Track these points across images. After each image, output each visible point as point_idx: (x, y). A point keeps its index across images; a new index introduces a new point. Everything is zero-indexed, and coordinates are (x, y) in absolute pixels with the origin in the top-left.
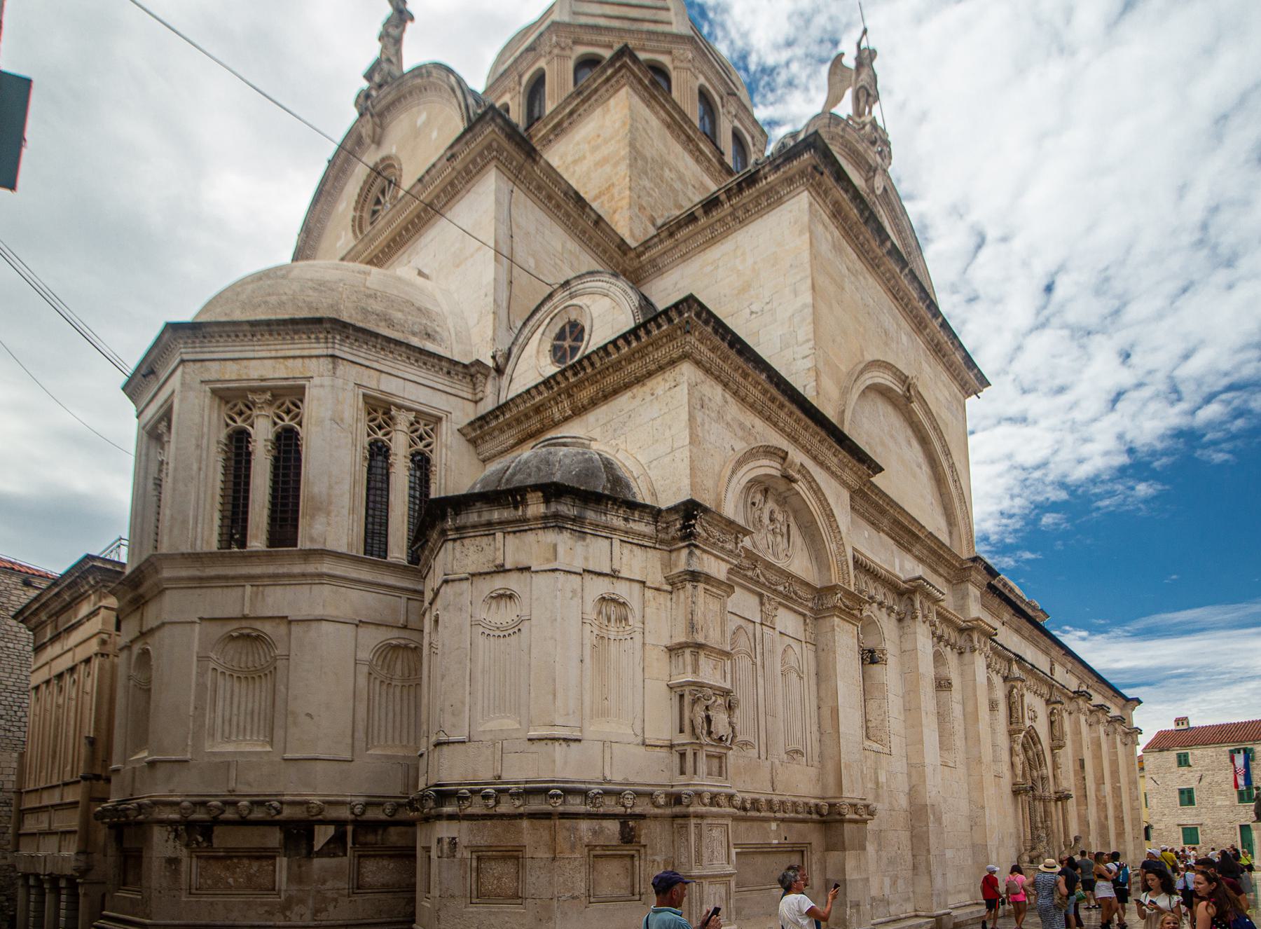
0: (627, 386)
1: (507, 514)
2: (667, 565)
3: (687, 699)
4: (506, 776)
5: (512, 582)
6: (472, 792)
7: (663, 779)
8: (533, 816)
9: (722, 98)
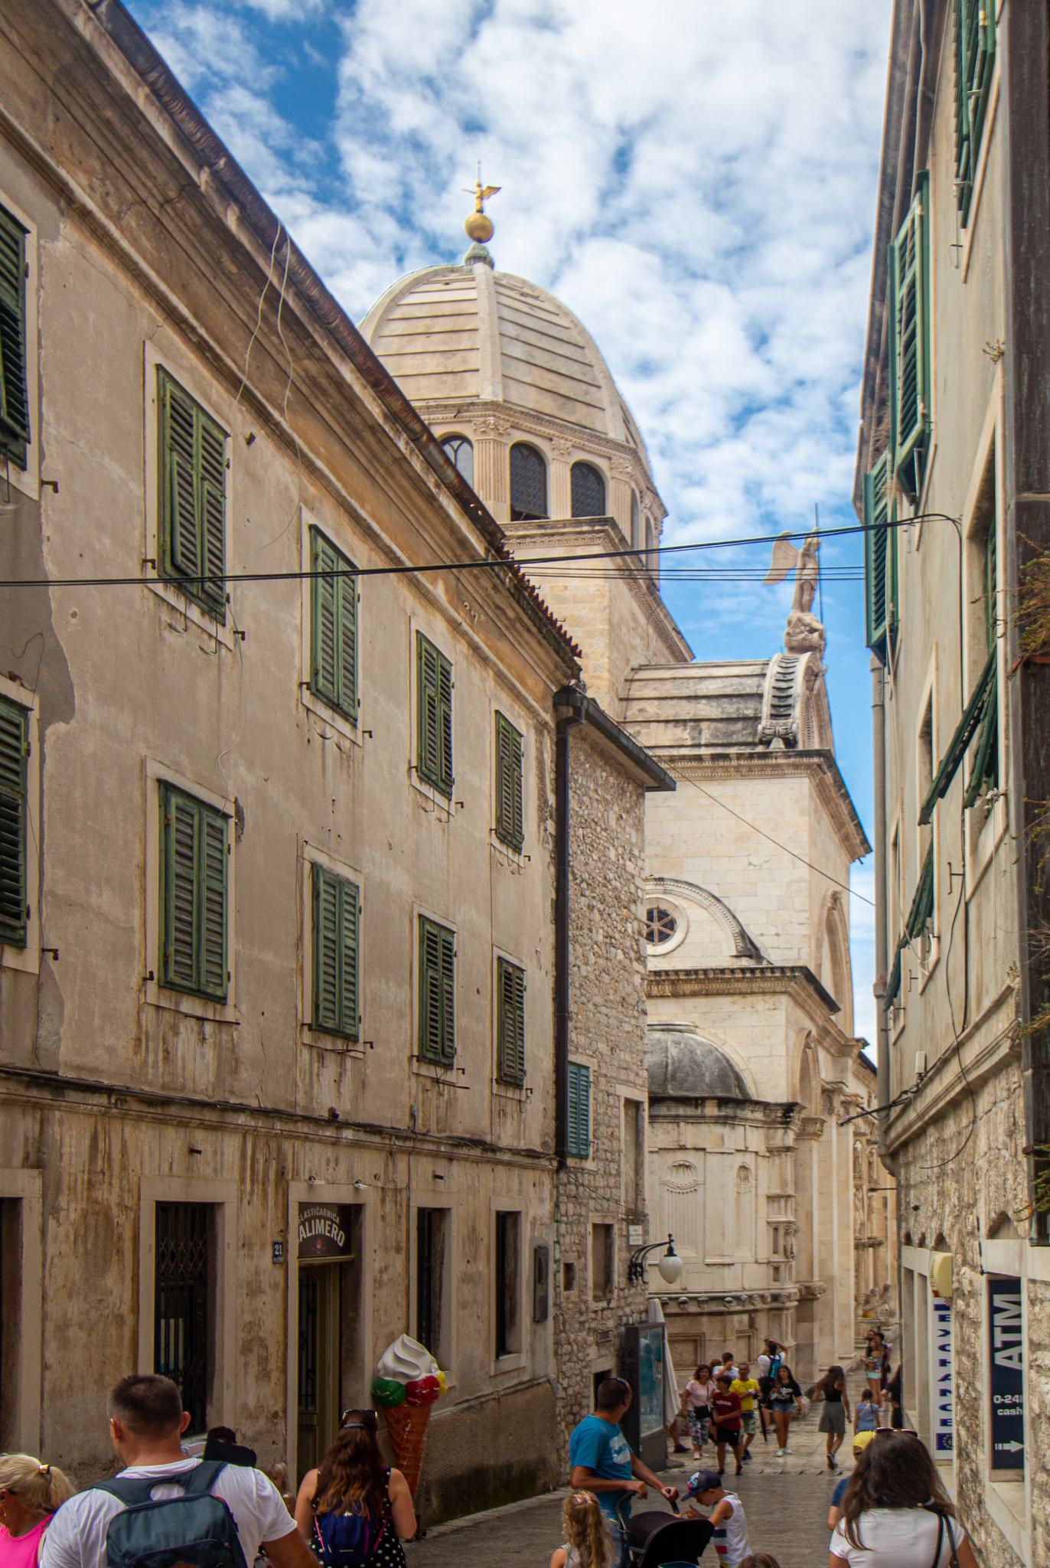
0: (729, 994)
1: (690, 1111)
2: (767, 1138)
3: (781, 1232)
4: (691, 1288)
5: (690, 1157)
6: (670, 1299)
7: (764, 1285)
8: (711, 1314)
9: (641, 492)
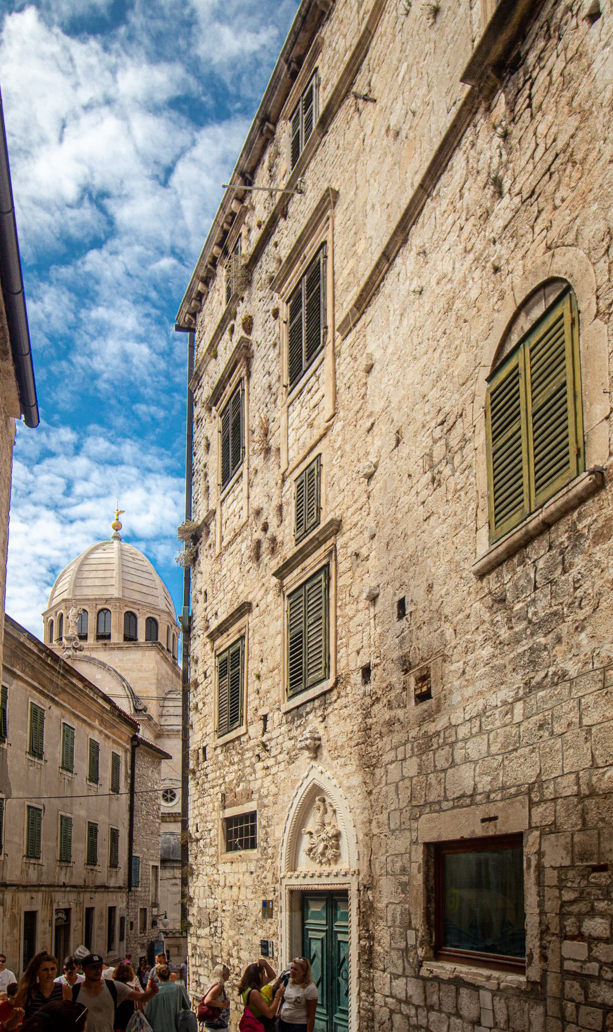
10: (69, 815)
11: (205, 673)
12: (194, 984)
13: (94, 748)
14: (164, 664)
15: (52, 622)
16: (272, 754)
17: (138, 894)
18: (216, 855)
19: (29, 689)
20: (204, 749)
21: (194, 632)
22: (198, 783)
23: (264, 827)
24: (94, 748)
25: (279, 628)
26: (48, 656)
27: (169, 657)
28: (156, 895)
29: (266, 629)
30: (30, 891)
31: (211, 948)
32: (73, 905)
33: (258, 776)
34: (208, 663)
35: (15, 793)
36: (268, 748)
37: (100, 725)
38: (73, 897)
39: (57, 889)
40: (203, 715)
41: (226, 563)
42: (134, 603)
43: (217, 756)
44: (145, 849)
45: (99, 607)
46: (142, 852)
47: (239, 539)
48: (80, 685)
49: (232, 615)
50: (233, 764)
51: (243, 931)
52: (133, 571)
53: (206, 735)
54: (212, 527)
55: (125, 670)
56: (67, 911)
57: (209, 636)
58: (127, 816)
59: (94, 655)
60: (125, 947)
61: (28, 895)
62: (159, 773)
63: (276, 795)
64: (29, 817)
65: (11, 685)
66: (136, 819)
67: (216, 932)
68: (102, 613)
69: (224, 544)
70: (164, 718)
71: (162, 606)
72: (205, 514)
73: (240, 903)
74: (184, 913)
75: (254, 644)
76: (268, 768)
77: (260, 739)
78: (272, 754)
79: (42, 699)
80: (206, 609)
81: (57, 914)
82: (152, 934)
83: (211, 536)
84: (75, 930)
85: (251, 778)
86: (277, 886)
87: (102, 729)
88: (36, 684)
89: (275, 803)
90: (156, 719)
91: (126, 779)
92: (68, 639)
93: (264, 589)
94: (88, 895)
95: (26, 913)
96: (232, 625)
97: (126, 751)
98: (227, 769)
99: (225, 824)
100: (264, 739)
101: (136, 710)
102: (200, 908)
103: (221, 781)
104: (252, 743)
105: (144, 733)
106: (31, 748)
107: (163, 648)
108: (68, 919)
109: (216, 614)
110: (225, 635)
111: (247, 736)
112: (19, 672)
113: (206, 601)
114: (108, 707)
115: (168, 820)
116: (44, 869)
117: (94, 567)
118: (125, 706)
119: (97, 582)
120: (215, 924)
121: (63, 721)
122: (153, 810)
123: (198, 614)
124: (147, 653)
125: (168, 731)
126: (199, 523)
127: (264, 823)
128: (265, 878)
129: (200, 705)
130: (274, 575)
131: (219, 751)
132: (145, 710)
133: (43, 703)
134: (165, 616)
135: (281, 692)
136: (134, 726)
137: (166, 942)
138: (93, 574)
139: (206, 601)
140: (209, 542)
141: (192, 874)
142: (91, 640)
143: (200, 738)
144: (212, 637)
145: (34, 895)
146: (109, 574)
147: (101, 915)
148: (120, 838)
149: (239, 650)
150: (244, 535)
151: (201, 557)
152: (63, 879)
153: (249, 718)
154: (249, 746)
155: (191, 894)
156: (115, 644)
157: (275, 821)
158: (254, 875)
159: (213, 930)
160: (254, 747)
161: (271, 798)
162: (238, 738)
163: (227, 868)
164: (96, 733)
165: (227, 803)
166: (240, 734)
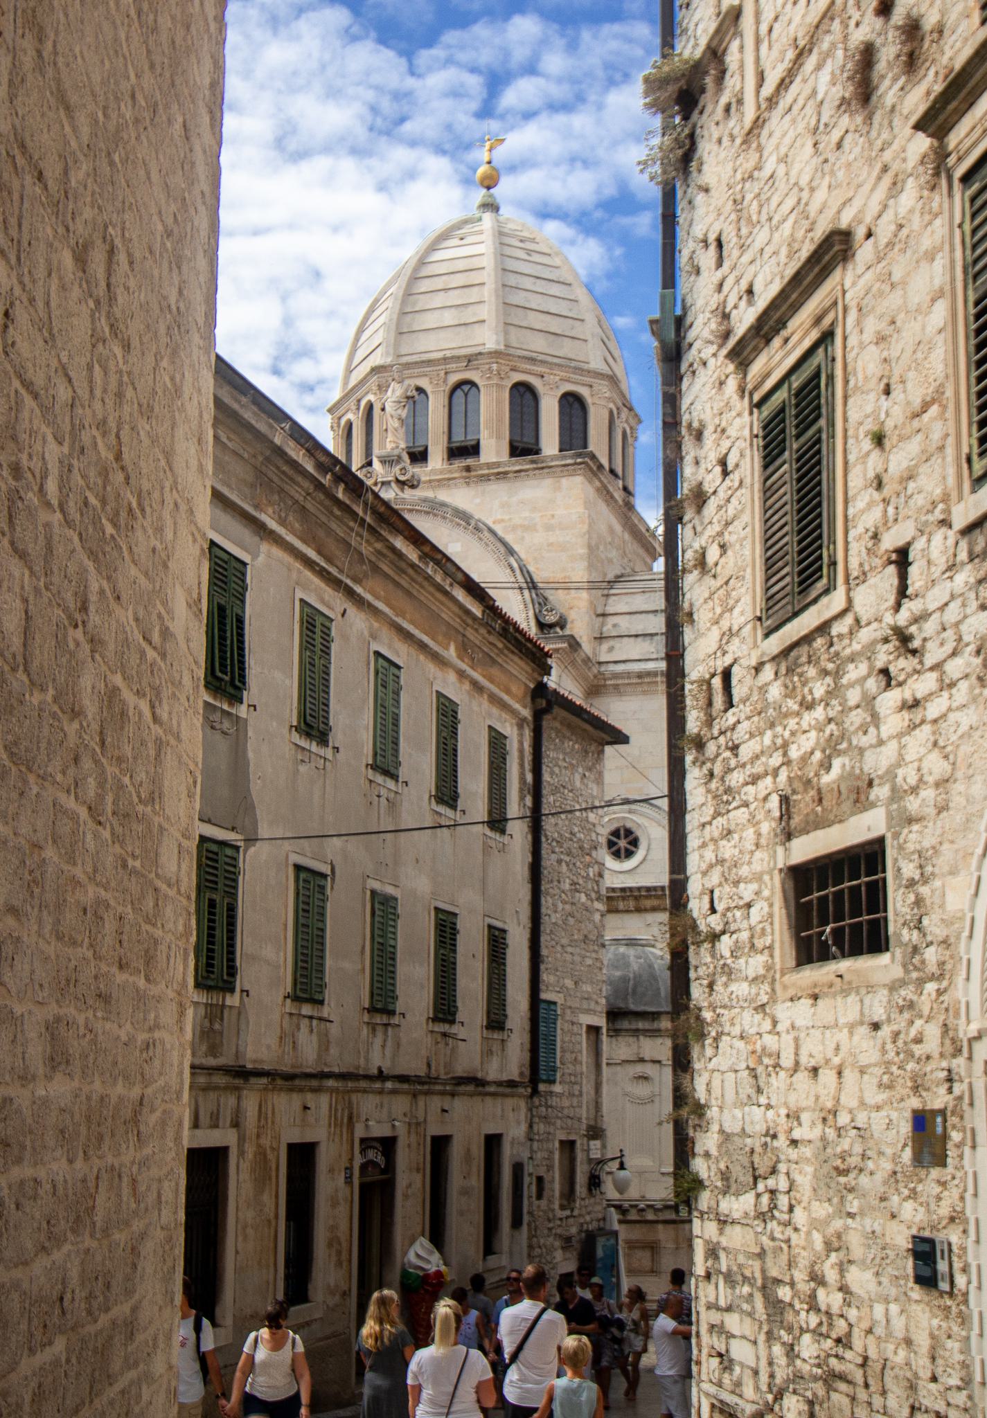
4: (648, 1196)
10: (390, 890)
11: (723, 463)
12: (715, 1362)
13: (447, 714)
14: (602, 507)
15: (350, 426)
16: (929, 661)
17: (554, 1101)
18: (767, 977)
19: (298, 565)
20: (727, 675)
21: (691, 356)
22: (711, 774)
23: (912, 883)
24: (447, 714)
25: (937, 282)
26: (338, 479)
27: (616, 489)
28: (598, 1106)
29: (899, 292)
30: (301, 1090)
31: (762, 1255)
32: (401, 1129)
33: (887, 730)
34: (732, 432)
35: (264, 832)
36: (916, 644)
37: (460, 657)
38: (400, 1105)
39: (363, 1084)
40: (720, 581)
41: (774, 141)
42: (532, 360)
43: (763, 689)
44: (569, 983)
45: (454, 379)
46: (563, 989)
47: (811, 62)
48: (412, 554)
49: (797, 278)
50: (810, 706)
51: (854, 1205)
52: (528, 283)
53: (731, 634)
54: (732, 59)
55: (514, 528)
56: (388, 1145)
57: (734, 354)
58: (524, 892)
59: (443, 496)
60: (525, 1243)
61: (296, 1100)
62: (599, 780)
63: (942, 783)
64: (297, 894)
65: (255, 556)
66: (546, 903)
67: (773, 1207)
68: (459, 393)
69: (767, 90)
70: (605, 646)
71: (597, 364)
72: (713, 26)
73: (843, 1119)
74: (683, 1149)
75: (862, 346)
76: (916, 704)
77: (889, 619)
78: (929, 661)
79: (328, 592)
80: (721, 285)
81: (363, 1151)
82: (588, 1211)
83: (731, 82)
84: (406, 1196)
85: (865, 741)
86: (959, 1063)
87: (464, 666)
88: (312, 554)
89: (942, 809)
90: (587, 647)
91: (522, 798)
92: (387, 461)
93: (887, 180)
94: (436, 1103)
95: (292, 1147)
96: (796, 308)
97: (521, 723)
98: (792, 723)
99: (790, 885)
100: (903, 618)
101: (542, 626)
102: (726, 1136)
103: (776, 760)
104: (865, 635)
105: (560, 680)
106: (302, 715)
107: (600, 467)
108: (390, 1167)
109: (750, 292)
110: (777, 342)
111: (849, 620)
112: (272, 525)
113: (720, 263)
114: (477, 610)
115: (621, 905)
116: (334, 1030)
117: (439, 283)
118: (516, 607)
119: (448, 318)
120: (771, 1183)
121: (375, 646)
122: (587, 877)
123: (700, 303)
124: (564, 481)
125: (616, 676)
126: (698, 53)
127: (909, 870)
128: (918, 1040)
129: (713, 554)
130: (918, 127)
131: (768, 672)
132: (562, 623)
133: (329, 601)
134: (604, 388)
135: (951, 471)
136: (538, 659)
137: (624, 1233)
138: (439, 300)
139: (720, 263)
140: (724, 100)
141: (702, 1036)
142: (437, 459)
143: (714, 646)
144: (741, 355)
145: (310, 1098)
146: (473, 295)
147: (468, 1157)
148: (509, 952)
149: (817, 375)
150: (825, 46)
151: (706, 149)
152: (377, 1059)
153: (854, 563)
154: (856, 647)
155: (701, 1094)
156: (489, 465)
157: (943, 862)
158: (886, 1031)
159: (765, 1199)
160: (874, 643)
161: (928, 794)
162: (824, 628)
163: (801, 1013)
164: (452, 677)
165: (796, 821)
166: (827, 615)
